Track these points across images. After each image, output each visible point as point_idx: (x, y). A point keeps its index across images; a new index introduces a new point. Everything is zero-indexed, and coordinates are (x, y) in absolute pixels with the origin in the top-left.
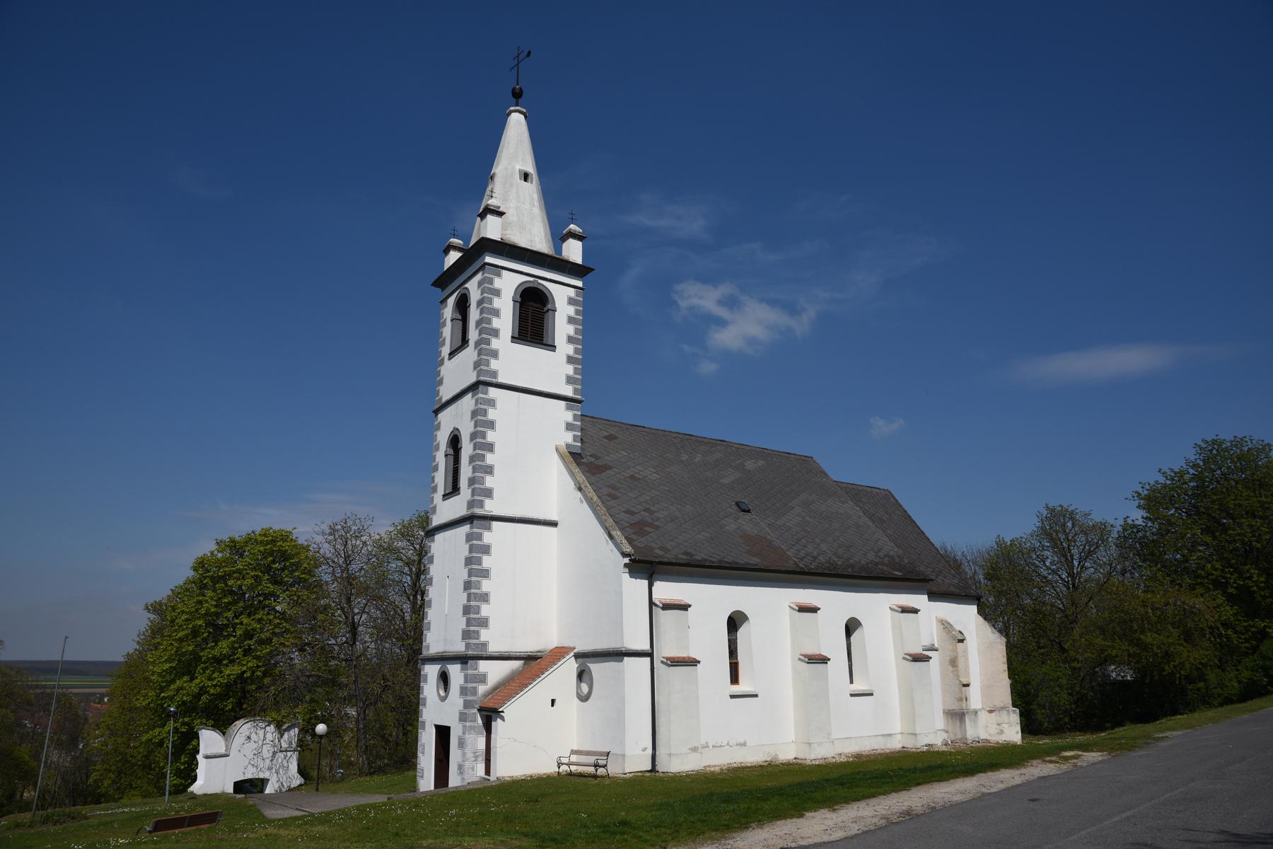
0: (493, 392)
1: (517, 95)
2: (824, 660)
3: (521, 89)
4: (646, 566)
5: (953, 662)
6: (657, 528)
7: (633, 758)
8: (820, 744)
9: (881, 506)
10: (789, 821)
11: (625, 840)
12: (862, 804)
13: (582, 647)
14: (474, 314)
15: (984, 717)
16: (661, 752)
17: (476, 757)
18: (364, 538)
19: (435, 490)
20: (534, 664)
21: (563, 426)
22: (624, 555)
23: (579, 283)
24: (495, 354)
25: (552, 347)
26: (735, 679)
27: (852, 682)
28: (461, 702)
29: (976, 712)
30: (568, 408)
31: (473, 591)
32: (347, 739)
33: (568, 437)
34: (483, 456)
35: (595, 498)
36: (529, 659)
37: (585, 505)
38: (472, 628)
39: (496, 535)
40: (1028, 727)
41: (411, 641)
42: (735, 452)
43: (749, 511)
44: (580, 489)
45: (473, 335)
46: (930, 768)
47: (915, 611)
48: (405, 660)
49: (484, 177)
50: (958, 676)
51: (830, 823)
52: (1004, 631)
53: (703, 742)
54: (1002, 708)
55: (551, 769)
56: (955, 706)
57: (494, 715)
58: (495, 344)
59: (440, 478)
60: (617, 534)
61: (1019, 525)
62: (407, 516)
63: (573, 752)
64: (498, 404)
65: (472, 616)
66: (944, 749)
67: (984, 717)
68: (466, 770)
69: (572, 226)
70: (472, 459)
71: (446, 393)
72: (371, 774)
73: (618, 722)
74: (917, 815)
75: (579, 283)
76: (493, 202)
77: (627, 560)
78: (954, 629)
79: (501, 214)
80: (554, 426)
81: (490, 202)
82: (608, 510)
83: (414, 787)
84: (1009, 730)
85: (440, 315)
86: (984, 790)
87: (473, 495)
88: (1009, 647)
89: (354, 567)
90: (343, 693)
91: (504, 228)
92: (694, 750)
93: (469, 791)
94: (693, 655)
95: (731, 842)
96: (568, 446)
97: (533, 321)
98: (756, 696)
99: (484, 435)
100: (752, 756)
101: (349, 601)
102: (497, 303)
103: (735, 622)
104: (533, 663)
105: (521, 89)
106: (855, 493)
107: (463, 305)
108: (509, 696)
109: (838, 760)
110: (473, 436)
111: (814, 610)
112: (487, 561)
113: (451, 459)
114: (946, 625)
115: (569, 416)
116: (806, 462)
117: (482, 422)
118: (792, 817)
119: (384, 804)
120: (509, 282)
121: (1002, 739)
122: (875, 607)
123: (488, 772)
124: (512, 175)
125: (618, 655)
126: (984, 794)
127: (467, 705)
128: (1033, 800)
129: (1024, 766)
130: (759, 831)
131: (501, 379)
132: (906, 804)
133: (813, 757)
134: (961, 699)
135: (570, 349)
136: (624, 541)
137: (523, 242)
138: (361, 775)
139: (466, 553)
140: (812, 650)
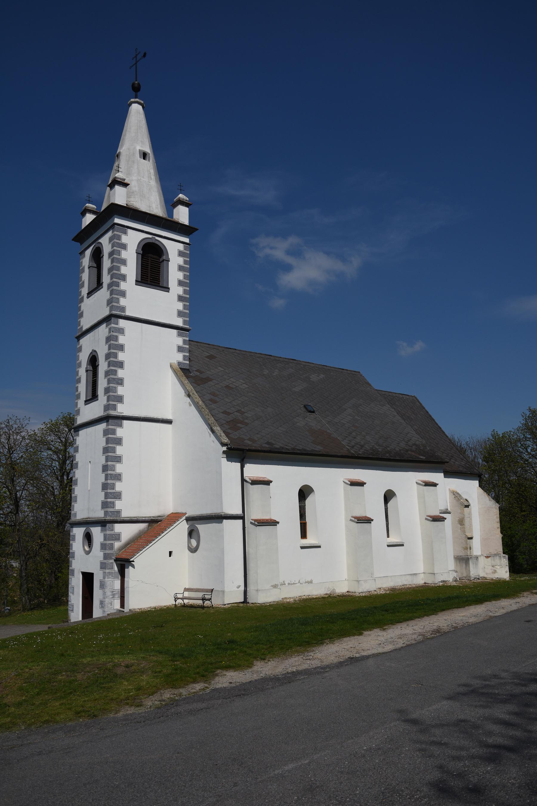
0: (122, 323)
1: (136, 89)
2: (369, 521)
3: (139, 84)
4: (238, 453)
5: (461, 522)
6: (247, 424)
7: (231, 594)
8: (365, 581)
9: (410, 408)
10: (352, 638)
11: (234, 654)
12: (404, 625)
14: (106, 263)
15: (482, 561)
16: (251, 588)
17: (113, 596)
18: (23, 434)
19: (78, 397)
20: (156, 526)
21: (176, 349)
22: (223, 444)
23: (187, 240)
24: (123, 294)
26: (304, 535)
27: (388, 536)
28: (101, 554)
29: (477, 558)
30: (179, 335)
31: (109, 472)
32: (11, 584)
33: (179, 357)
34: (116, 371)
35: (201, 403)
36: (153, 522)
37: (193, 407)
38: (109, 500)
39: (126, 430)
40: (514, 568)
41: (60, 510)
42: (304, 368)
43: (313, 412)
44: (189, 396)
45: (106, 279)
46: (449, 598)
47: (435, 485)
48: (55, 524)
49: (112, 155)
50: (464, 532)
51: (382, 639)
52: (497, 499)
53: (281, 581)
54: (496, 555)
55: (169, 602)
56: (462, 553)
57: (126, 564)
58: (123, 286)
59: (82, 388)
60: (217, 429)
61: (509, 422)
62: (55, 415)
63: (186, 590)
64: (126, 332)
65: (109, 491)
66: (454, 584)
67: (482, 561)
68: (106, 605)
69: (181, 196)
70: (107, 373)
71: (86, 323)
72: (32, 609)
73: (219, 567)
74: (445, 633)
75: (187, 240)
76: (119, 175)
77: (225, 448)
78: (462, 498)
79: (126, 185)
80: (170, 348)
81: (117, 175)
82: (210, 411)
83: (66, 618)
84: (501, 571)
85: (79, 264)
86: (491, 614)
87: (108, 401)
88: (500, 509)
89: (15, 455)
90: (8, 550)
91: (129, 196)
92: (275, 586)
93: (110, 620)
94: (369, 515)
95: (312, 654)
96: (179, 363)
97: (152, 269)
98: (319, 547)
99: (116, 355)
100: (317, 591)
101: (13, 481)
102: (124, 254)
103: (304, 493)
104: (155, 525)
105: (139, 84)
106: (391, 399)
107: (97, 256)
108: (139, 549)
109: (379, 592)
110: (108, 356)
111: (361, 484)
112: (119, 450)
113: (91, 374)
114: (456, 495)
115: (180, 341)
116: (355, 376)
117: (114, 346)
118: (354, 635)
119: (46, 632)
120: (133, 238)
121: (495, 576)
122: (406, 483)
123: (122, 605)
124: (134, 154)
125: (219, 518)
126: (491, 617)
128: (529, 621)
129: (518, 597)
130: (331, 646)
131: (128, 313)
132: (436, 624)
133: (361, 590)
134: (466, 548)
135: (180, 291)
136: (223, 434)
137: (143, 208)
138: (24, 610)
139: (104, 444)
140: (359, 513)
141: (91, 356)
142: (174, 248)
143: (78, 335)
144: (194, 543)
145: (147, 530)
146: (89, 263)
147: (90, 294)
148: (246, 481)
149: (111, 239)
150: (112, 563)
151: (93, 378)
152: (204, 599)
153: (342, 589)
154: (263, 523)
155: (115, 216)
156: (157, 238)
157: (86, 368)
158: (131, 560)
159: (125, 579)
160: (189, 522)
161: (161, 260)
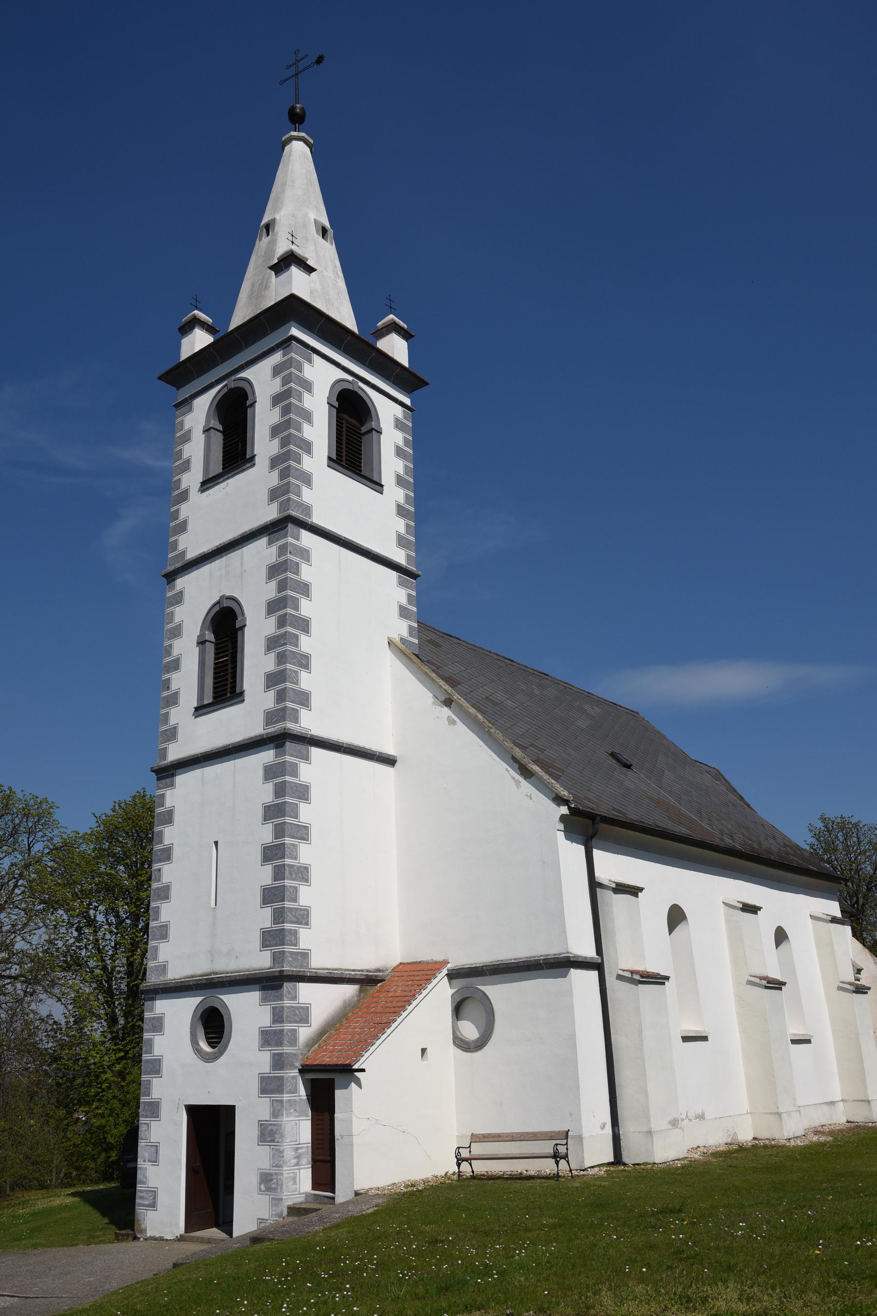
1: (297, 119)
4: (588, 826)
13: (458, 960)
16: (627, 1129)
17: (298, 1157)
20: (381, 994)
22: (559, 800)
23: (407, 401)
25: (377, 485)
30: (401, 584)
36: (367, 981)
39: (317, 769)
45: (263, 445)
57: (338, 1078)
63: (476, 1138)
75: (407, 401)
77: (564, 810)
79: (310, 270)
98: (705, 1038)
104: (372, 990)
120: (323, 375)
124: (305, 226)
127: (278, 1062)
131: (317, 519)
133: (787, 1135)
141: (217, 608)
142: (388, 410)
143: (171, 568)
144: (470, 1031)
145: (359, 1001)
146: (208, 420)
147: (207, 484)
148: (601, 886)
149: (277, 370)
150: (294, 1077)
151: (216, 659)
152: (556, 1156)
153: (745, 1136)
154: (648, 977)
155: (292, 323)
156: (361, 384)
157: (202, 635)
158: (355, 1067)
159: (338, 1116)
160: (454, 981)
161: (364, 429)
